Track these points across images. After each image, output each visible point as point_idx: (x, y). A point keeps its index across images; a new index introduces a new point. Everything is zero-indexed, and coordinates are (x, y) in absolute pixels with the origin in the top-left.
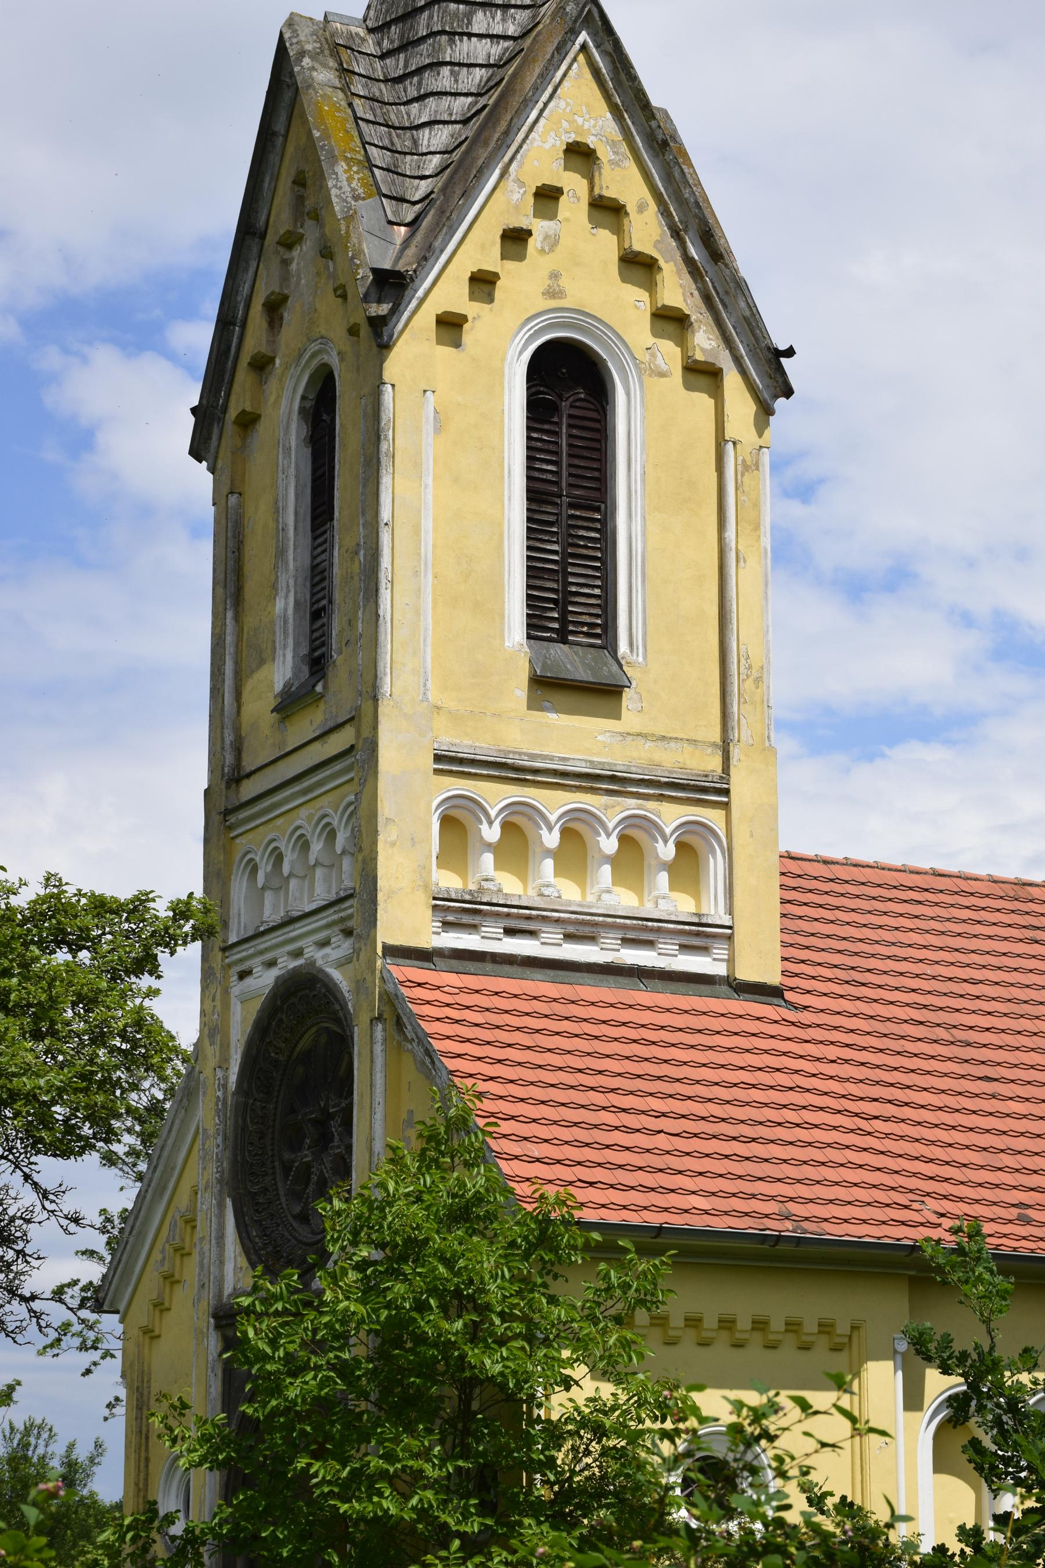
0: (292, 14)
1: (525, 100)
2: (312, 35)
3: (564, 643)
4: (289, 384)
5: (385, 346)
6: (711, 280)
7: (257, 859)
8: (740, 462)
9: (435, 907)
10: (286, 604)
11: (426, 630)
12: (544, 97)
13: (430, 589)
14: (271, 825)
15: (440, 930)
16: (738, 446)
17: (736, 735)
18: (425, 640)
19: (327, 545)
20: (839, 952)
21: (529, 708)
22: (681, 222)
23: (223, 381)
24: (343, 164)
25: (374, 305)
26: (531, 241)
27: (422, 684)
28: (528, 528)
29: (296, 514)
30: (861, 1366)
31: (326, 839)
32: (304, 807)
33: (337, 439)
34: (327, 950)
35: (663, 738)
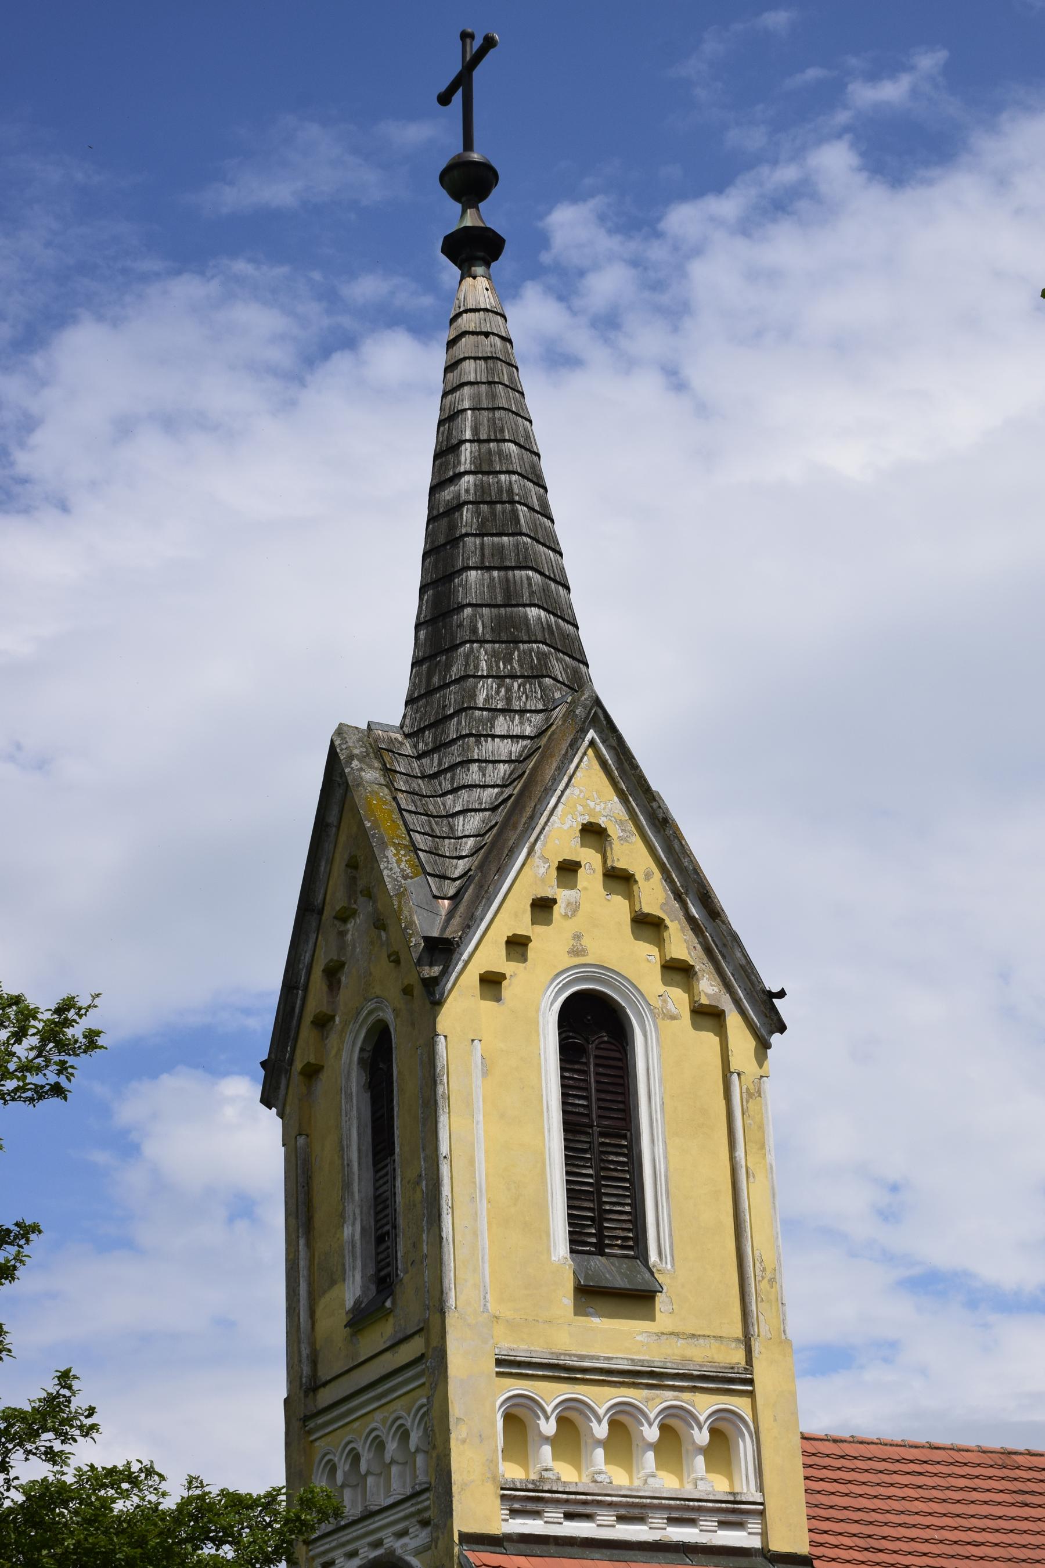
0: (340, 724)
1: (546, 789)
2: (359, 741)
3: (602, 1255)
4: (349, 1038)
5: (437, 1003)
6: (710, 935)
7: (336, 1460)
8: (744, 1090)
9: (503, 1497)
10: (354, 1231)
11: (483, 1248)
12: (561, 787)
13: (485, 1213)
14: (348, 1428)
15: (508, 1517)
16: (742, 1077)
17: (756, 1330)
18: (483, 1258)
19: (389, 1177)
20: (856, 1522)
21: (576, 1314)
22: (682, 886)
23: (289, 1037)
24: (392, 849)
25: (427, 968)
26: (556, 908)
27: (482, 1297)
28: (566, 1155)
29: (359, 1151)
31: (400, 1438)
32: (378, 1411)
33: (395, 1084)
34: (405, 1540)
35: (693, 1336)
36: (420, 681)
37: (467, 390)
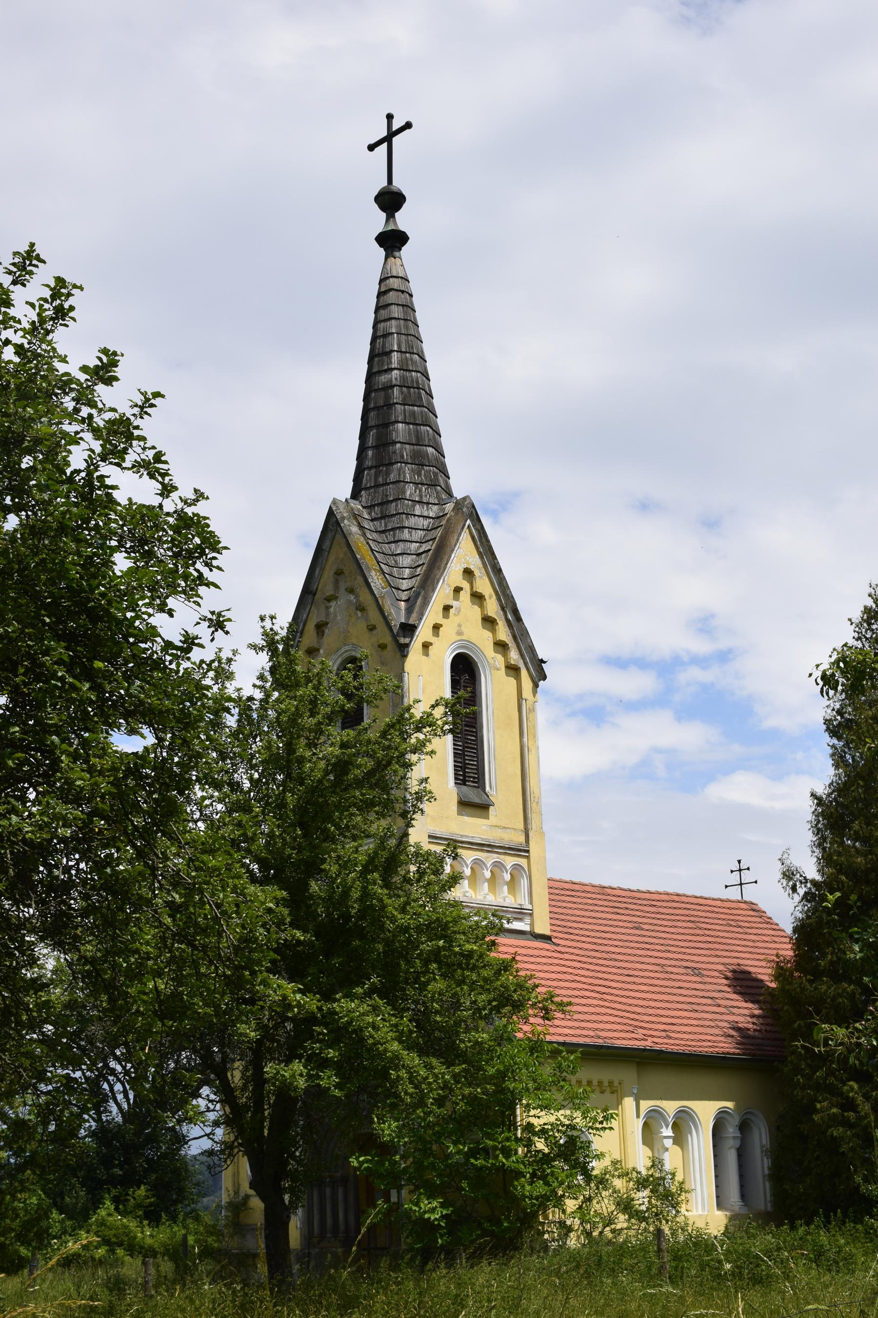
5: (404, 656)
30: (622, 1099)
35: (504, 828)
36: (370, 478)
37: (393, 322)
